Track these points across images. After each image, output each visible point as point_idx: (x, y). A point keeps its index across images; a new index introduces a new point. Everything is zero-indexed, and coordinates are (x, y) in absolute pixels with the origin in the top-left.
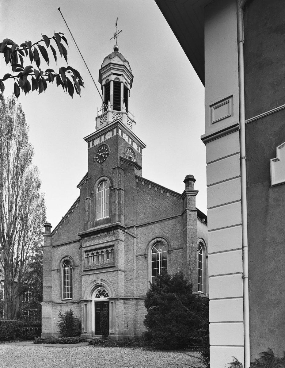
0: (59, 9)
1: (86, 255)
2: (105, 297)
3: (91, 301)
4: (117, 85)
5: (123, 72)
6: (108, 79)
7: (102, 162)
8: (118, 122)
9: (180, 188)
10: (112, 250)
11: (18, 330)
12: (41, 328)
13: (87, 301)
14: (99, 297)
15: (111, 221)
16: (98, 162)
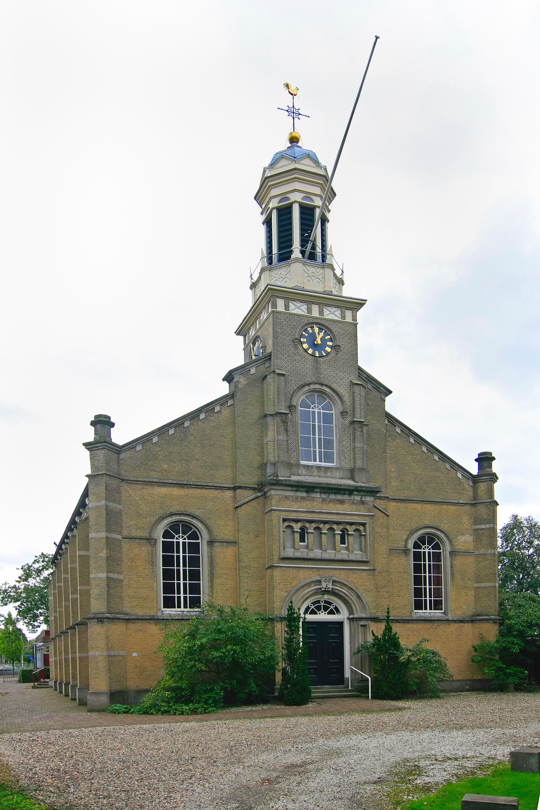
0: (377, 38)
1: (285, 526)
2: (331, 612)
4: (307, 212)
5: (271, 189)
6: (288, 199)
9: (473, 469)
11: (29, 567)
14: (313, 612)
15: (290, 463)
16: (306, 351)
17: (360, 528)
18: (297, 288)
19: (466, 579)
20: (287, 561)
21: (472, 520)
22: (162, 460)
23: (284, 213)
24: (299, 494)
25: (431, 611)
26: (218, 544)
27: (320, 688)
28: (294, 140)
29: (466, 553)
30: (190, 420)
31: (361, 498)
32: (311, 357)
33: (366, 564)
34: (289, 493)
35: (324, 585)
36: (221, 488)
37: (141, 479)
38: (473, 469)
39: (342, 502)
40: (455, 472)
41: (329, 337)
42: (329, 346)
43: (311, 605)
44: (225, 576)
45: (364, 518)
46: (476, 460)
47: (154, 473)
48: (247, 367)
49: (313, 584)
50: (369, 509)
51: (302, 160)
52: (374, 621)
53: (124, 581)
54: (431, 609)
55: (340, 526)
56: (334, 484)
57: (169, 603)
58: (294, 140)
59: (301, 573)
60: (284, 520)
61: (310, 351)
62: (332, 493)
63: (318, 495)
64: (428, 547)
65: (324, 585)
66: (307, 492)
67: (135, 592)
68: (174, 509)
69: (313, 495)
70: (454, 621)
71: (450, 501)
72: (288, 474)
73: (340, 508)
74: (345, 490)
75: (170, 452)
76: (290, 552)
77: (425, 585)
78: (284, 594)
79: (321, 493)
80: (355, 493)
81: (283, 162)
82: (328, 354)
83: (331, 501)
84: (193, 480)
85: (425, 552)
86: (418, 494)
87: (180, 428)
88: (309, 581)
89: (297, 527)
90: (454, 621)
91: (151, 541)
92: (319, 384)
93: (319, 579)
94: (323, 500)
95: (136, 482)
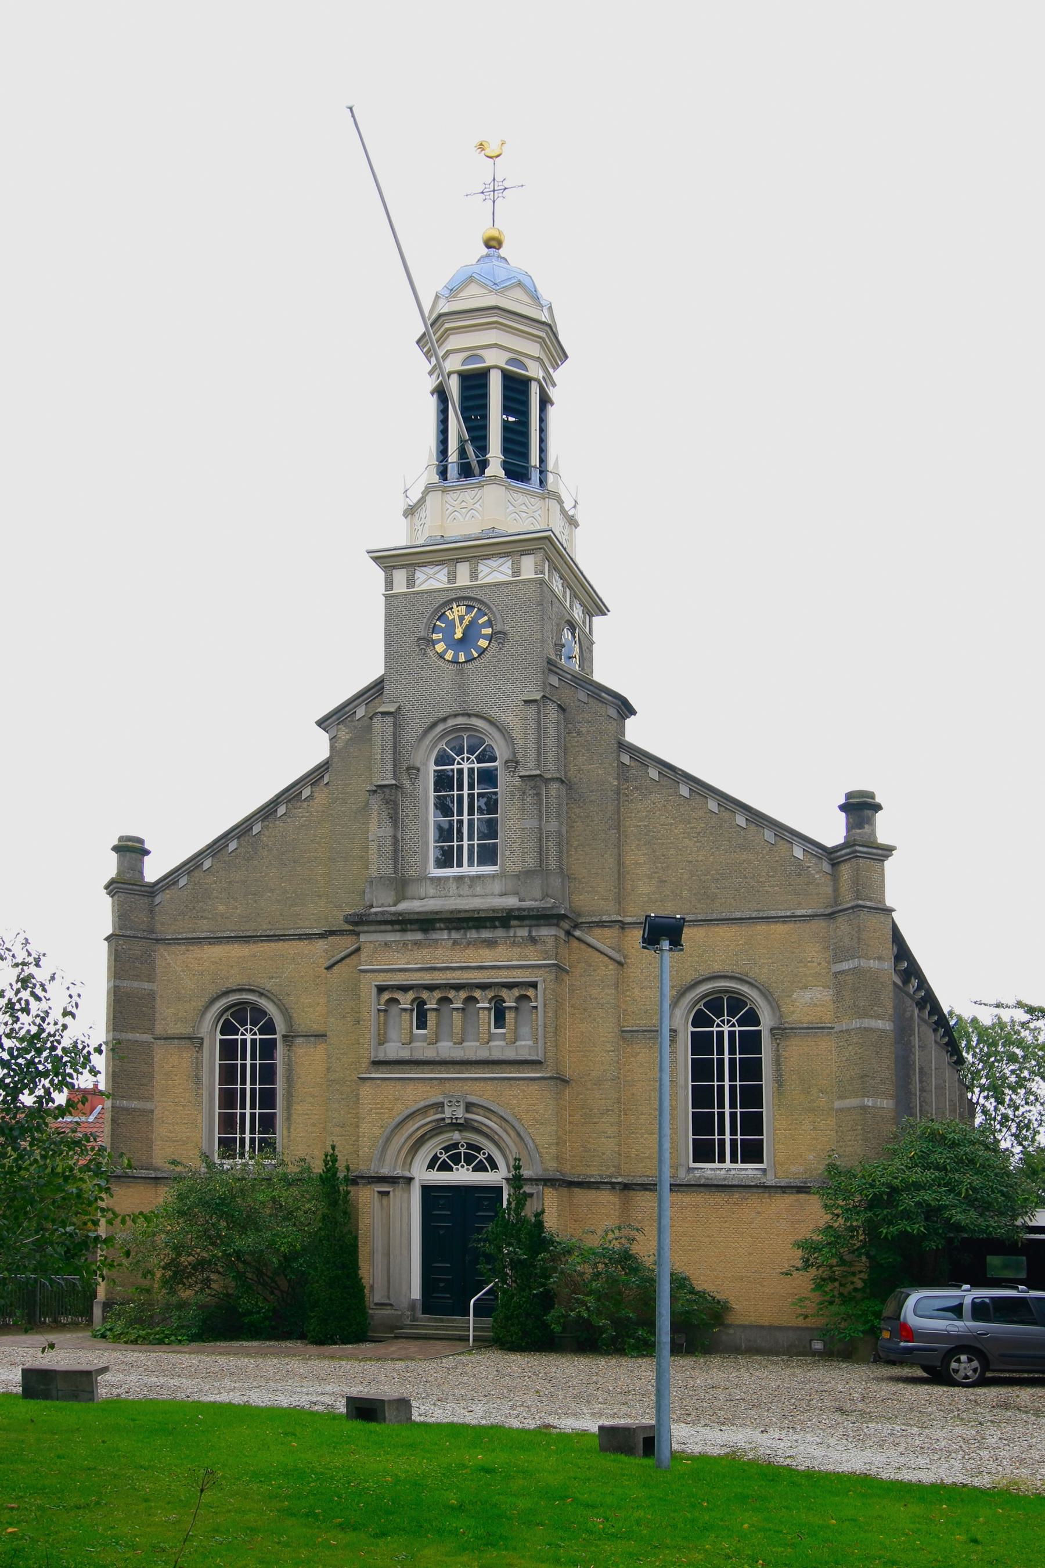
0: (351, 109)
1: (383, 1001)
2: (480, 1168)
3: (409, 1180)
7: (462, 659)
8: (548, 538)
9: (831, 830)
10: (524, 998)
12: (645, 1348)
13: (392, 1180)
14: (445, 1167)
16: (441, 656)
17: (528, 994)
18: (430, 542)
19: (814, 1091)
20: (383, 1068)
21: (831, 953)
22: (217, 898)
23: (474, 383)
24: (410, 936)
25: (734, 1166)
26: (301, 1039)
27: (448, 1321)
28: (493, 243)
29: (815, 1029)
30: (262, 821)
31: (530, 932)
32: (451, 667)
33: (538, 1067)
34: (390, 937)
35: (448, 1113)
36: (309, 937)
37: (184, 935)
38: (831, 830)
39: (491, 943)
40: (789, 845)
41: (486, 618)
42: (484, 637)
43: (441, 1153)
44: (311, 1100)
45: (536, 971)
46: (842, 808)
47: (205, 922)
48: (347, 709)
49: (432, 1112)
50: (546, 952)
51: (462, 290)
52: (553, 1186)
53: (156, 1112)
54: (734, 1160)
55: (487, 992)
56: (466, 911)
57: (703, 1152)
58: (493, 243)
59: (409, 1091)
60: (381, 989)
61: (449, 656)
62: (470, 928)
63: (445, 935)
64: (729, 1021)
65: (448, 1113)
66: (425, 931)
67: (170, 1132)
68: (232, 984)
69: (435, 935)
70: (784, 1189)
71: (773, 913)
72: (390, 901)
73: (487, 957)
74: (492, 919)
75: (230, 882)
76: (393, 1050)
77: (721, 1105)
78: (377, 1131)
79: (449, 929)
80: (513, 923)
81: (473, 289)
82: (482, 652)
83: (469, 944)
84: (264, 927)
85: (723, 1032)
86: (698, 906)
87: (246, 839)
88: (422, 1104)
89: (406, 1000)
90: (784, 1189)
91: (195, 1041)
92: (463, 715)
93: (441, 1100)
94: (455, 943)
95: (176, 941)
